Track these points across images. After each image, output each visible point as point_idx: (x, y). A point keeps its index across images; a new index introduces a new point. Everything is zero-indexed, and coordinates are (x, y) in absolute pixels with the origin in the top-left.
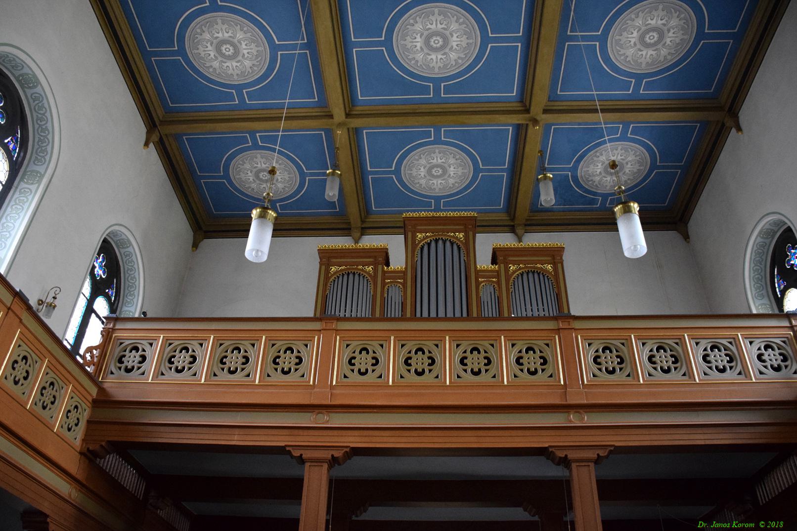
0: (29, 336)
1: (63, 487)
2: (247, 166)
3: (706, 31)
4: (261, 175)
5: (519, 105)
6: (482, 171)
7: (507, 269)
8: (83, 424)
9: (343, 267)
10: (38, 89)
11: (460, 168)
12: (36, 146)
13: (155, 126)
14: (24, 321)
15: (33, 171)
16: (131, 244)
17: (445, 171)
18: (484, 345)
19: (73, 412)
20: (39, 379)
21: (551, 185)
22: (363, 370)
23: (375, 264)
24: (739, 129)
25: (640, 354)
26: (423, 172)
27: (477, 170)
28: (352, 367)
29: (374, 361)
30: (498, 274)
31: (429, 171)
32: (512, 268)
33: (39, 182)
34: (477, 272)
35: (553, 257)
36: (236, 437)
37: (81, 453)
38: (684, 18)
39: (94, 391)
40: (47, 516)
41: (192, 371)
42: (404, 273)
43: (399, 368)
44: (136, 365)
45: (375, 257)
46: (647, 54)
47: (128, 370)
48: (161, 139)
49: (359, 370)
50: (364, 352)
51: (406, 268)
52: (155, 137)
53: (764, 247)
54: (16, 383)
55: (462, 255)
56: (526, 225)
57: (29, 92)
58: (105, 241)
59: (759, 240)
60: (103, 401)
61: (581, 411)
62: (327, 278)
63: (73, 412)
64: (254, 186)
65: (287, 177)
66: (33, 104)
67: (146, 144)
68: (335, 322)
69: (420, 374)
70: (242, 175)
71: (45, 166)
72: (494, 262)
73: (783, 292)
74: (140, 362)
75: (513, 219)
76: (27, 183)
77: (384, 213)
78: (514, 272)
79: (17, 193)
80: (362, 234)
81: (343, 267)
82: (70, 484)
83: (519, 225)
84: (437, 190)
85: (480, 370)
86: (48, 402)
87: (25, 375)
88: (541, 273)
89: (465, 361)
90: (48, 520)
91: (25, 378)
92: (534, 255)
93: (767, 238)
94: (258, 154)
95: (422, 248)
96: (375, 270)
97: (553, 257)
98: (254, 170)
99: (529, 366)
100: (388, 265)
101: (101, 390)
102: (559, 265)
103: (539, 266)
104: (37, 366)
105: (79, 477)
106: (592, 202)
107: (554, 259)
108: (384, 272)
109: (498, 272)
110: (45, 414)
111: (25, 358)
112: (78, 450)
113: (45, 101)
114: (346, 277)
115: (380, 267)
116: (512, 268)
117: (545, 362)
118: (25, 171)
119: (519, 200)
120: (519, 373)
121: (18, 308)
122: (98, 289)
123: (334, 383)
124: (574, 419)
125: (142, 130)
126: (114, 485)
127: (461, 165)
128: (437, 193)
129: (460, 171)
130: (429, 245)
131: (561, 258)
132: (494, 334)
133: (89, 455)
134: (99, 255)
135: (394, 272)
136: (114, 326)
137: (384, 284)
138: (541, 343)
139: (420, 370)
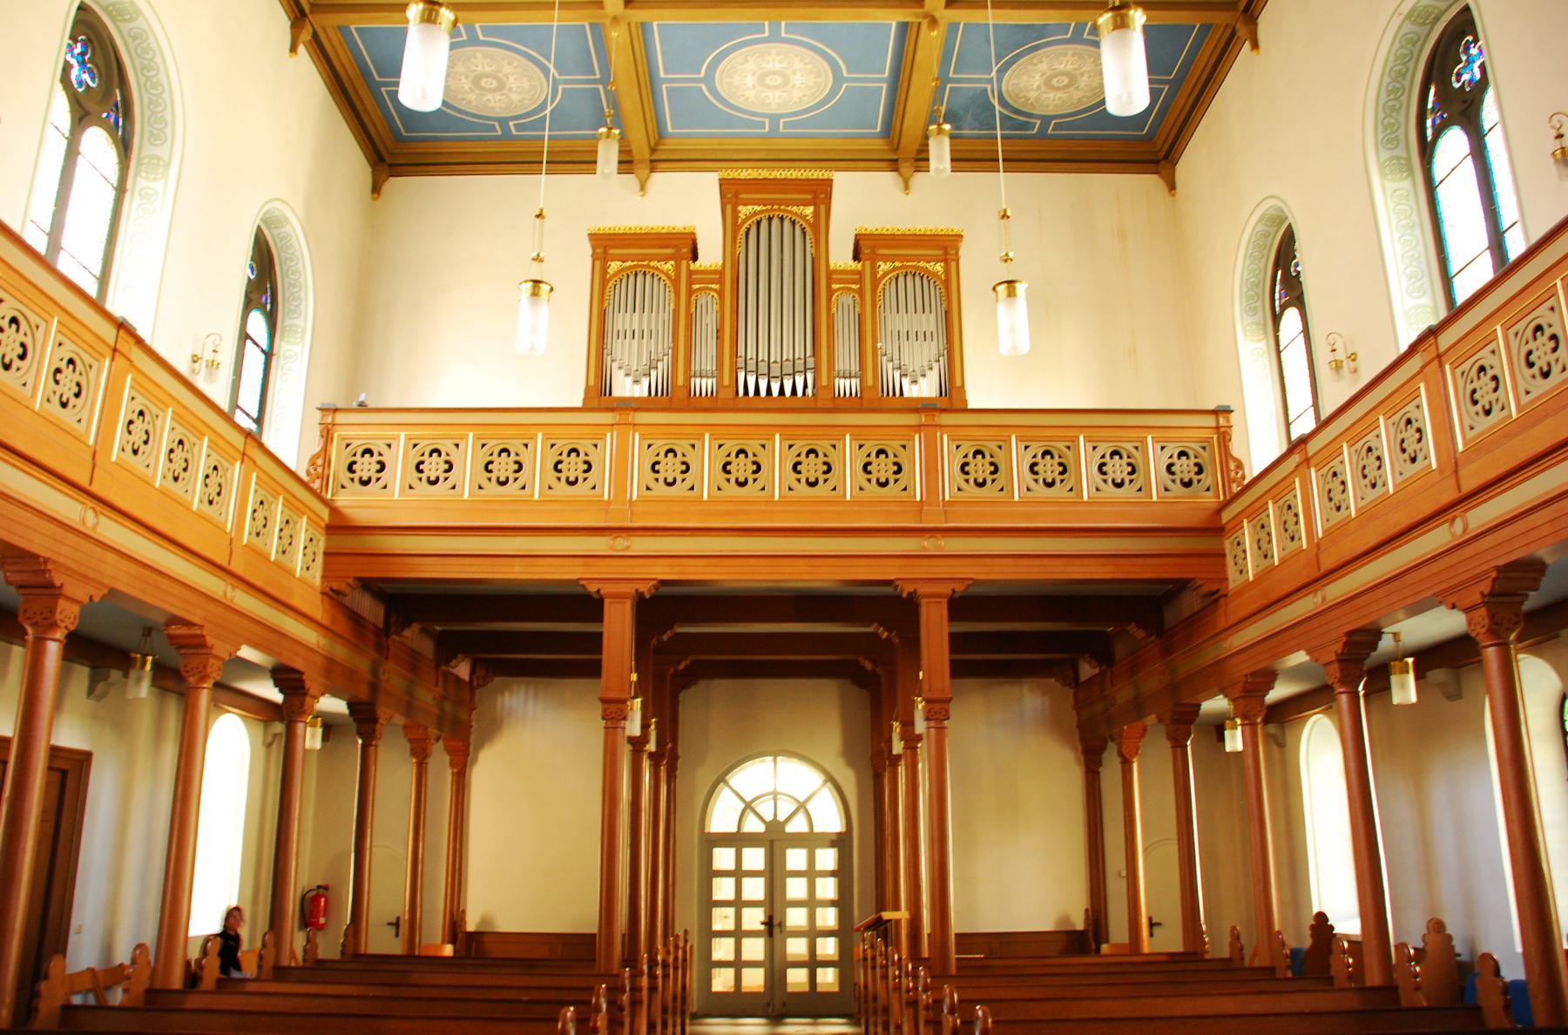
0: (221, 443)
1: (310, 636)
4: (483, 82)
6: (847, 80)
7: (874, 270)
8: (320, 558)
9: (629, 263)
10: (140, 23)
12: (147, 113)
13: (303, 13)
14: (137, 363)
15: (150, 157)
16: (288, 222)
17: (786, 80)
18: (822, 446)
19: (178, 450)
20: (202, 466)
21: (946, 141)
23: (677, 258)
24: (1255, 46)
25: (1017, 459)
26: (750, 80)
27: (838, 79)
30: (859, 277)
31: (761, 79)
32: (884, 267)
33: (303, 338)
34: (830, 273)
35: (945, 249)
36: (517, 569)
37: (323, 593)
39: (325, 513)
40: (302, 673)
41: (450, 483)
42: (721, 273)
47: (365, 483)
48: (315, 36)
51: (724, 265)
52: (306, 35)
53: (1414, 43)
54: (64, 405)
56: (917, 160)
57: (125, 27)
58: (259, 228)
59: (1408, 27)
60: (339, 526)
62: (604, 281)
63: (178, 450)
64: (472, 97)
65: (526, 85)
66: (132, 46)
67: (293, 49)
71: (168, 145)
72: (856, 257)
73: (1438, 133)
75: (896, 150)
76: (146, 179)
77: (688, 136)
78: (885, 274)
79: (137, 198)
80: (652, 170)
81: (629, 263)
83: (906, 160)
86: (69, 394)
87: (20, 351)
88: (925, 275)
91: (22, 357)
92: (916, 247)
93: (1423, 24)
94: (479, 52)
96: (677, 268)
97: (945, 249)
100: (695, 257)
101: (334, 511)
102: (953, 265)
103: (922, 264)
104: (92, 374)
105: (326, 621)
106: (1026, 126)
107: (946, 253)
108: (690, 273)
109: (860, 273)
110: (137, 462)
111: (71, 361)
113: (151, 40)
114: (632, 279)
115: (684, 263)
118: (139, 159)
119: (905, 126)
121: (126, 345)
122: (82, 116)
125: (282, 22)
126: (355, 618)
129: (811, 80)
130: (759, 223)
131: (957, 254)
132: (836, 432)
133: (332, 595)
134: (74, 38)
137: (690, 292)
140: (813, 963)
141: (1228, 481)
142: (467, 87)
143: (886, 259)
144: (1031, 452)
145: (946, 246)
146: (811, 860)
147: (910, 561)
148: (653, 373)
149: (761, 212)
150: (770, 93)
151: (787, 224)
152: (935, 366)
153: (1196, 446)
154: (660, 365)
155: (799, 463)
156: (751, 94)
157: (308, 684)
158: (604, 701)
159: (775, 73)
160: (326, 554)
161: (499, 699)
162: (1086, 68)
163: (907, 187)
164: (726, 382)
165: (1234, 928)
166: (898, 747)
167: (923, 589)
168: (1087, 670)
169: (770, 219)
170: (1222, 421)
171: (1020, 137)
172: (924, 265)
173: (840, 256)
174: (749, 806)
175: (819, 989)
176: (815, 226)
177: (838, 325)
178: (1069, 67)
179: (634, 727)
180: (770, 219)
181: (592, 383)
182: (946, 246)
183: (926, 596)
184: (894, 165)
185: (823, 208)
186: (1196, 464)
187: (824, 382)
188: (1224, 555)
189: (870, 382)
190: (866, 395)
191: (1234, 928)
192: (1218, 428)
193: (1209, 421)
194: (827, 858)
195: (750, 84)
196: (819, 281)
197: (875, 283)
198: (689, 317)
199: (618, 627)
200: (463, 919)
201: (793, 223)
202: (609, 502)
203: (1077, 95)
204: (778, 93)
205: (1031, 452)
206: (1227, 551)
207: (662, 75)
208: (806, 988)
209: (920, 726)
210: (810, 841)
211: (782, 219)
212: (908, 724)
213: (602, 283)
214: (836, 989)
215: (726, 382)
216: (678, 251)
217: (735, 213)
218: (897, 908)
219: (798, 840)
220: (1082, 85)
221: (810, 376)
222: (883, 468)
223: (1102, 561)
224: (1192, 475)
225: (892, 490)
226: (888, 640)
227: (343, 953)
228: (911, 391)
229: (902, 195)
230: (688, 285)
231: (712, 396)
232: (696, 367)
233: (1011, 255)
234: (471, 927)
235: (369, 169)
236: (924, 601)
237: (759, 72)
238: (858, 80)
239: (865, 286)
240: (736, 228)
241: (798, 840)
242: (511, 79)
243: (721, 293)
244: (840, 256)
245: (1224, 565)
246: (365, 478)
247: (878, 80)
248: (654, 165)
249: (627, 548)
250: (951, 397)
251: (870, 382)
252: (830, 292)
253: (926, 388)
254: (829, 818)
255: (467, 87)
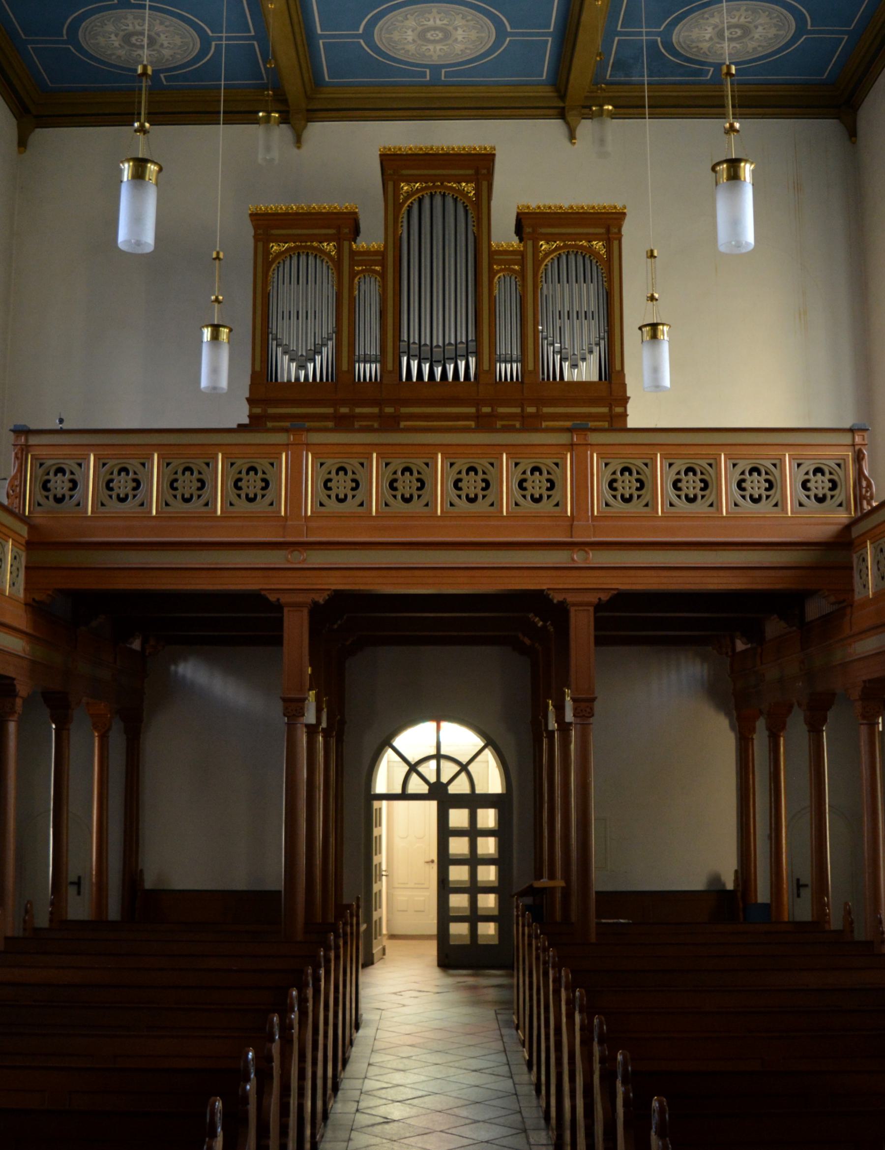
2: (110, 28)
3: (809, 28)
5: (548, 88)
7: (536, 249)
11: (474, 31)
22: (341, 496)
23: (338, 239)
25: (661, 477)
26: (410, 36)
28: (329, 492)
29: (354, 485)
32: (544, 246)
34: (492, 253)
37: (26, 604)
38: (778, 16)
39: (24, 531)
40: (14, 679)
42: (383, 254)
43: (383, 493)
44: (68, 494)
45: (339, 228)
46: (739, 18)
49: (337, 496)
50: (341, 473)
51: (386, 246)
55: (470, 223)
61: (586, 549)
64: (122, 52)
68: (305, 433)
69: (407, 500)
70: (101, 40)
74: (71, 489)
75: (562, 97)
78: (547, 254)
82: (21, 639)
84: (434, 10)
85: (476, 496)
89: (460, 484)
90: (15, 682)
95: (410, 208)
98: (122, 33)
99: (533, 491)
105: (29, 631)
108: (353, 253)
109: (523, 254)
112: (22, 602)
115: (346, 243)
116: (544, 246)
117: (552, 487)
120: (521, 500)
123: (309, 514)
124: (578, 558)
127: (474, 28)
128: (435, 60)
130: (420, 201)
133: (34, 607)
135: (367, 253)
136: (26, 440)
138: (549, 462)
139: (407, 496)
140: (474, 917)
141: (859, 498)
142: (116, 44)
143: (549, 239)
144: (675, 469)
145: (608, 224)
146: (473, 818)
147: (559, 573)
148: (318, 358)
149: (423, 189)
150: (431, 47)
151: (450, 202)
152: (596, 349)
153: (832, 464)
154: (324, 350)
155: (460, 480)
156: (412, 48)
157: (18, 687)
158: (284, 700)
159: (435, 29)
160: (27, 568)
161: (173, 668)
162: (761, 21)
163: (572, 136)
164: (390, 367)
165: (846, 904)
166: (553, 725)
167: (571, 598)
168: (740, 646)
169: (432, 196)
170: (858, 439)
171: (694, 83)
172: (588, 240)
173: (503, 234)
174: (413, 768)
175: (481, 942)
176: (477, 204)
177: (500, 308)
178: (742, 20)
179: (310, 717)
180: (432, 196)
181: (258, 368)
182: (608, 224)
183: (574, 605)
184: (562, 114)
185: (485, 183)
186: (830, 481)
187: (486, 367)
188: (852, 568)
189: (531, 367)
190: (526, 380)
191: (846, 904)
192: (853, 445)
193: (847, 439)
194: (488, 818)
195: (410, 39)
196: (481, 258)
197: (537, 263)
198: (352, 300)
199: (296, 628)
200: (142, 880)
201: (455, 200)
202: (286, 518)
203: (751, 45)
204: (438, 47)
205: (675, 469)
206: (855, 566)
207: (319, 32)
208: (467, 941)
209: (569, 717)
210: (473, 801)
211: (444, 196)
212: (560, 709)
213: (264, 267)
214: (496, 942)
215: (390, 367)
216: (339, 228)
217: (397, 190)
218: (552, 877)
219: (459, 801)
220: (757, 36)
221: (472, 361)
222: (537, 485)
223: (737, 572)
224: (826, 491)
225: (546, 506)
226: (544, 627)
227: (51, 921)
228: (571, 375)
229: (569, 144)
230: (348, 268)
231: (375, 384)
232: (360, 351)
233: (656, 296)
234: (148, 885)
235: (14, 121)
236: (572, 609)
237: (420, 29)
238: (523, 34)
239: (524, 268)
240: (398, 206)
241: (459, 801)
242: (163, 36)
243: (383, 275)
244: (503, 234)
245: (852, 577)
246: (59, 496)
247: (544, 34)
248: (314, 114)
249: (304, 561)
250: (611, 388)
251: (531, 367)
252: (492, 274)
253: (586, 372)
254: (490, 778)
255: (116, 44)
